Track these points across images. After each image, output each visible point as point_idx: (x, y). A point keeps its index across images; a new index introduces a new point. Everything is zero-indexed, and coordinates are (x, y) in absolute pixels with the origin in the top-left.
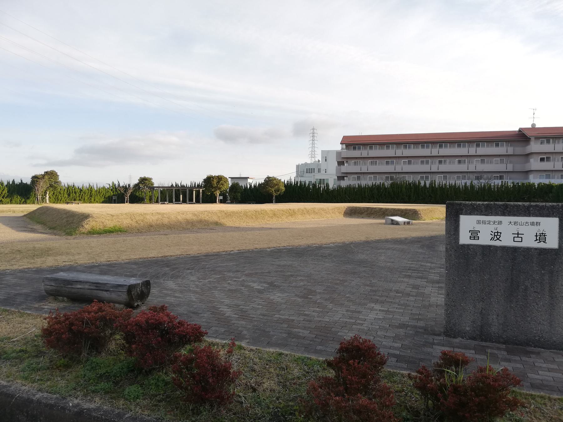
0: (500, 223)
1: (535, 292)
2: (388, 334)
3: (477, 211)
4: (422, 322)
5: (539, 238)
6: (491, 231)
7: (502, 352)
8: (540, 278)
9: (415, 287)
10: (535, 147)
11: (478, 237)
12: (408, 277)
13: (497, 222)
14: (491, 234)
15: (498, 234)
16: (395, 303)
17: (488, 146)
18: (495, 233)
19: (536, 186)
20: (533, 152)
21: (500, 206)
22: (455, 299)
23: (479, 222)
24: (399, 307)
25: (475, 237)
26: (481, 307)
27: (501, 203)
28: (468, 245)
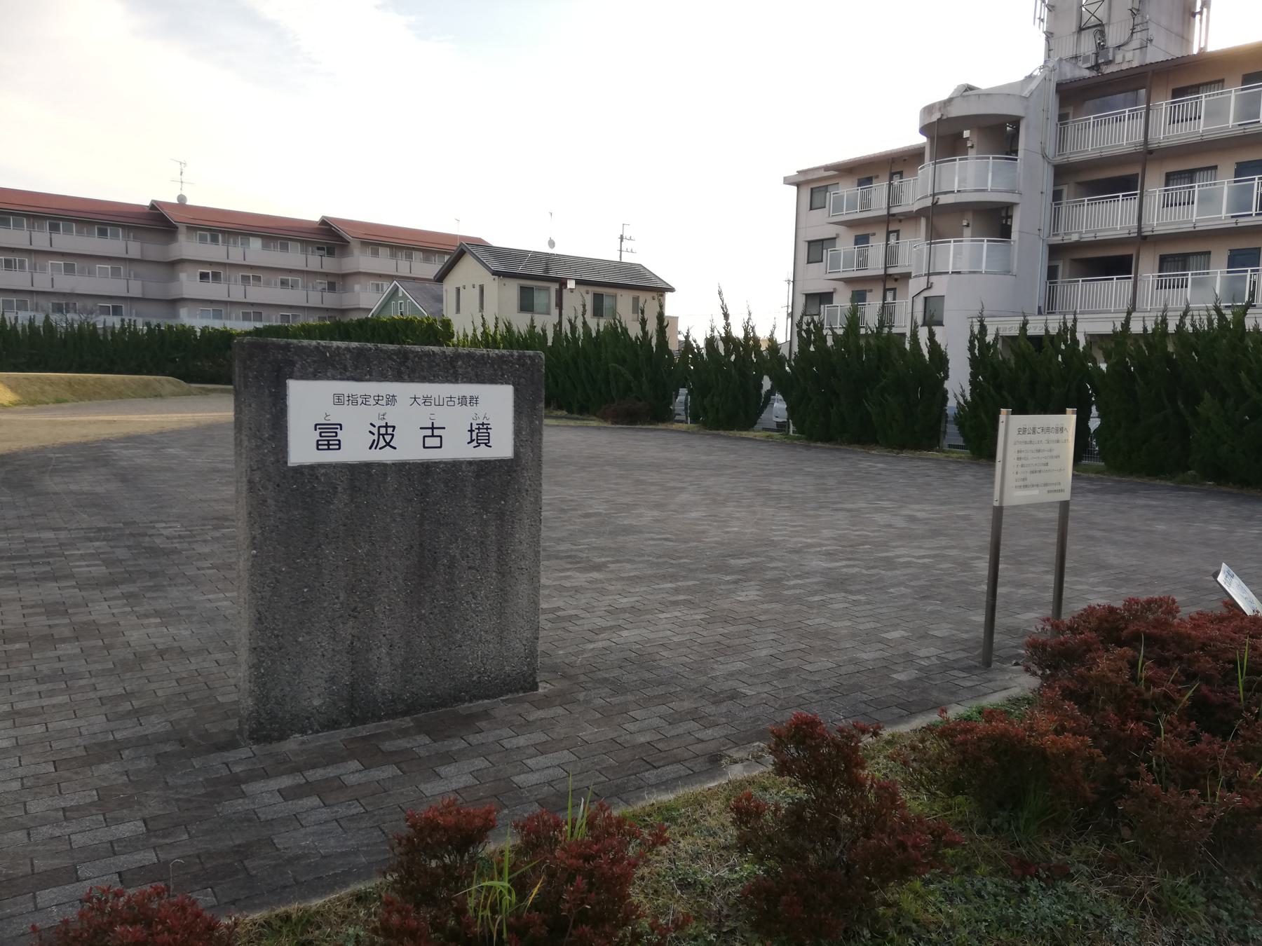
0: (392, 400)
1: (470, 568)
2: (71, 800)
3: (334, 367)
4: (153, 717)
5: (477, 436)
6: (371, 424)
7: (417, 738)
8: (478, 532)
9: (54, 609)
10: (187, 247)
11: (339, 441)
12: (10, 582)
13: (385, 399)
14: (370, 432)
15: (387, 430)
16: (20, 678)
17: (79, 232)
18: (379, 427)
19: (198, 334)
20: (184, 257)
21: (389, 355)
22: (280, 627)
23: (339, 399)
24: (43, 687)
25: (331, 442)
26: (351, 634)
27: (391, 347)
28: (312, 467)
